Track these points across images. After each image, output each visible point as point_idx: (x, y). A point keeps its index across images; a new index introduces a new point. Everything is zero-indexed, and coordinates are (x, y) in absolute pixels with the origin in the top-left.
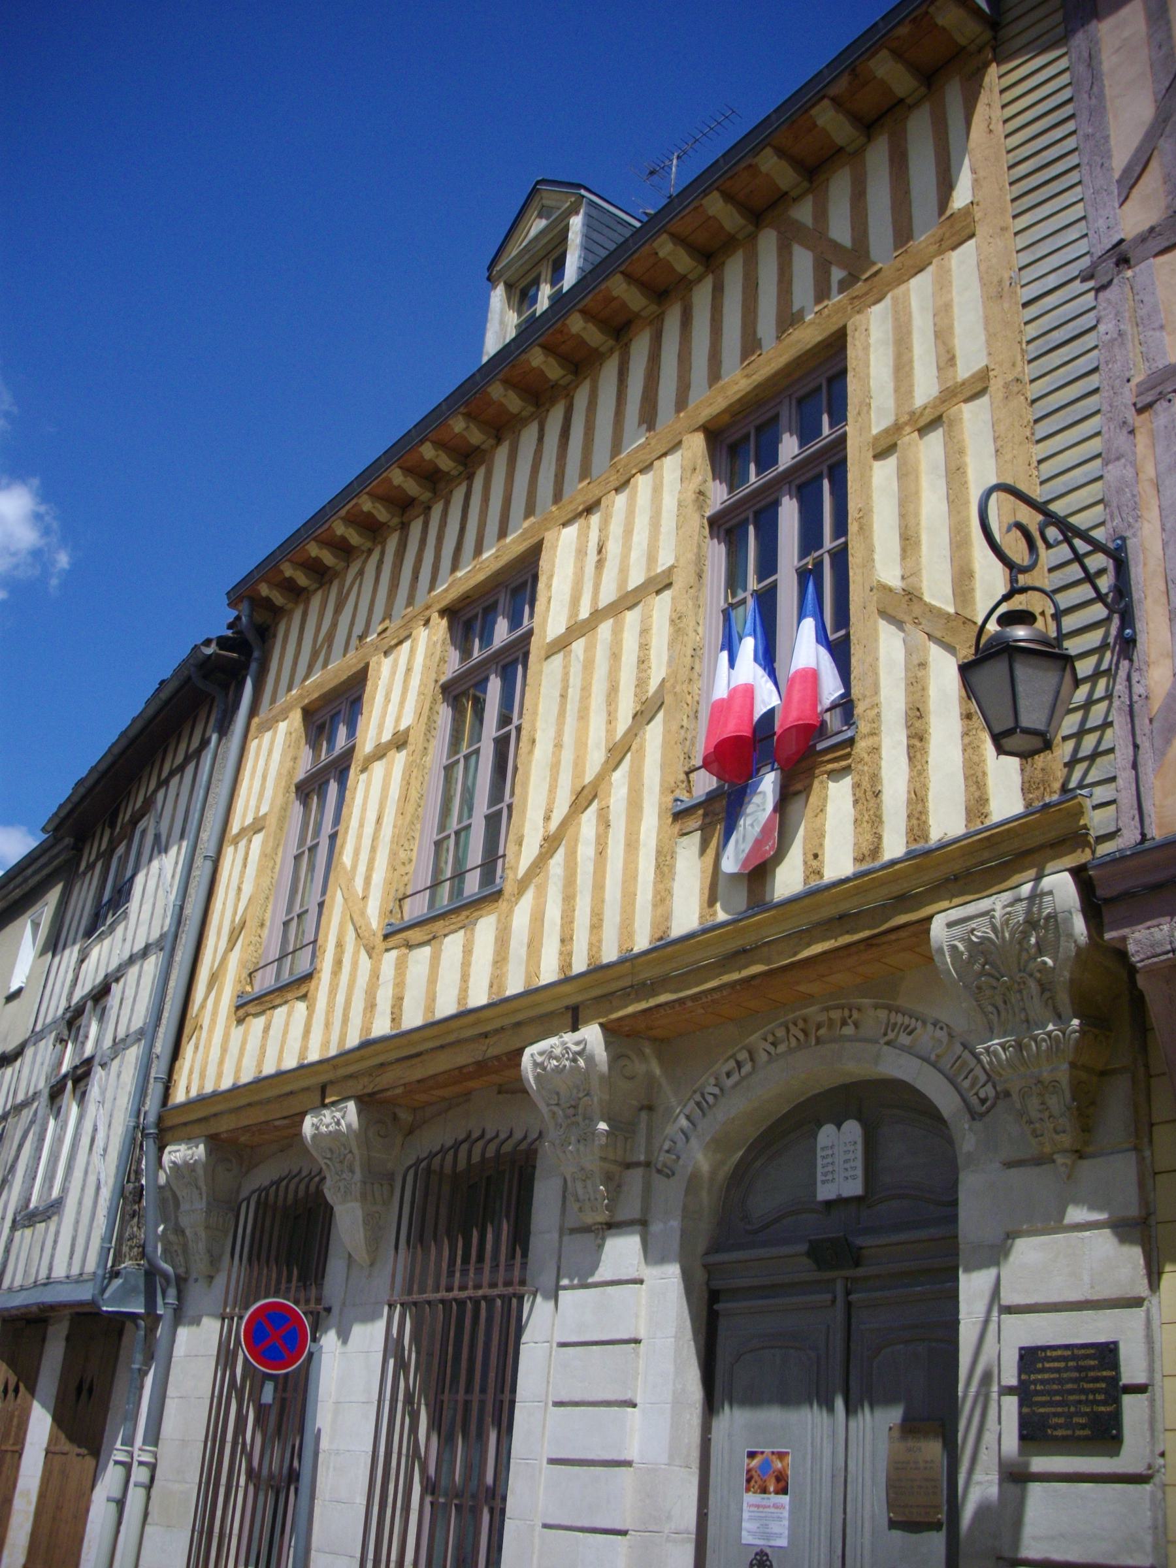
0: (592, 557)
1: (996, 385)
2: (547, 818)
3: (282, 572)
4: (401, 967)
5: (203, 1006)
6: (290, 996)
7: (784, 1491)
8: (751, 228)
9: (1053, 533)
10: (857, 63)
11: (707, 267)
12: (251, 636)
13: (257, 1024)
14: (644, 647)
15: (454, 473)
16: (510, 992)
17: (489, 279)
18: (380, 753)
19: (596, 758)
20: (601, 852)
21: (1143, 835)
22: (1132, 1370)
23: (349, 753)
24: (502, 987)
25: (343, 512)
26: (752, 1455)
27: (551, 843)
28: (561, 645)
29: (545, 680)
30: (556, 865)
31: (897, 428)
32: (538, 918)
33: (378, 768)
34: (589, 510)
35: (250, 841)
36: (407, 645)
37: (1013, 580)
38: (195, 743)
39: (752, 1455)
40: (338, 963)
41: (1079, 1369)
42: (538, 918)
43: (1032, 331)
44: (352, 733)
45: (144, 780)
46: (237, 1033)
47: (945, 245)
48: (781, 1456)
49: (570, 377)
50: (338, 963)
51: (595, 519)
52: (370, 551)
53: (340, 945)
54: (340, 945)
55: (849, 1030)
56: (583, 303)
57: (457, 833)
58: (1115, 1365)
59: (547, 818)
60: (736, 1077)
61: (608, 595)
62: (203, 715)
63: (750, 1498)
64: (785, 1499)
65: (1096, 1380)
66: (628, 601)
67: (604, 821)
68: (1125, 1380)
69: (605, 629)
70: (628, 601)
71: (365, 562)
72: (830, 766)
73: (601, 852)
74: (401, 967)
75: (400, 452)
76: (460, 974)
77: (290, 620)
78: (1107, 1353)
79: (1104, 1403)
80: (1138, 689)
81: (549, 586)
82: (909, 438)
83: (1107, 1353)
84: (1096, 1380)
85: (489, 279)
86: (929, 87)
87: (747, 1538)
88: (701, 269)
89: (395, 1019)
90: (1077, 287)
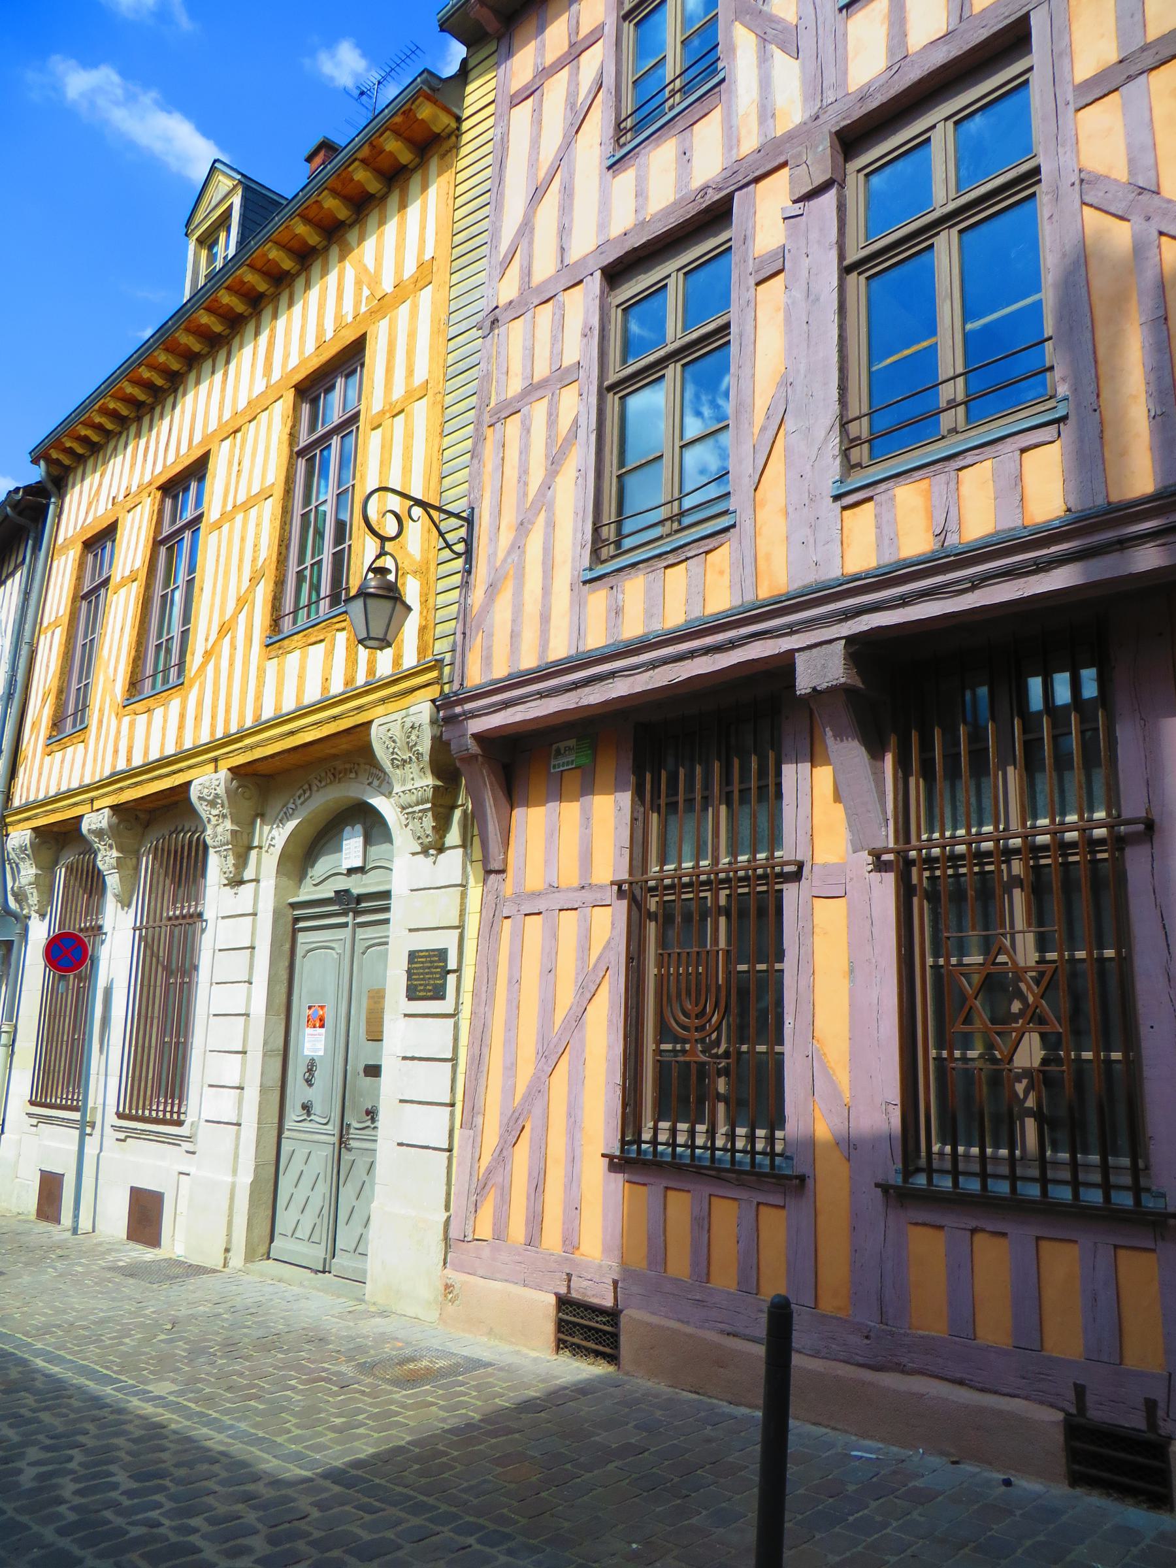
0: (235, 468)
1: (430, 393)
2: (207, 640)
3: (63, 443)
4: (132, 724)
5: (28, 743)
6: (75, 741)
7: (322, 1026)
8: (325, 243)
9: (417, 511)
10: (350, 169)
11: (302, 265)
12: (50, 486)
13: (59, 755)
14: (258, 536)
15: (203, 352)
16: (186, 747)
17: (186, 235)
18: (122, 584)
19: (231, 605)
20: (231, 665)
21: (461, 685)
22: (452, 964)
23: (198, 519)
24: (182, 744)
25: (97, 407)
26: (310, 1008)
27: (208, 654)
28: (218, 525)
29: (210, 545)
30: (210, 667)
31: (383, 412)
32: (200, 703)
33: (123, 591)
34: (235, 432)
35: (53, 633)
36: (139, 507)
37: (382, 547)
38: (20, 559)
39: (310, 1008)
40: (101, 722)
41: (431, 962)
42: (200, 703)
43: (451, 359)
44: (199, 502)
45: (13, 557)
46: (48, 759)
47: (419, 285)
48: (322, 1007)
49: (228, 331)
50: (101, 722)
51: (239, 435)
52: (120, 433)
53: (101, 710)
54: (101, 710)
55: (353, 775)
56: (228, 282)
57: (312, 565)
58: (445, 960)
59: (207, 640)
60: (302, 799)
61: (241, 498)
62: (15, 548)
63: (309, 1031)
64: (322, 1031)
65: (437, 967)
66: (246, 506)
67: (233, 647)
68: (449, 968)
69: (239, 517)
70: (246, 506)
71: (118, 441)
72: (338, 626)
73: (231, 665)
74: (132, 724)
75: (127, 371)
76: (157, 732)
77: (75, 475)
78: (442, 954)
79: (439, 979)
80: (469, 601)
81: (213, 484)
82: (387, 423)
83: (442, 954)
84: (437, 967)
85: (186, 235)
86: (422, 158)
87: (306, 1052)
88: (298, 267)
89: (129, 760)
90: (474, 333)
